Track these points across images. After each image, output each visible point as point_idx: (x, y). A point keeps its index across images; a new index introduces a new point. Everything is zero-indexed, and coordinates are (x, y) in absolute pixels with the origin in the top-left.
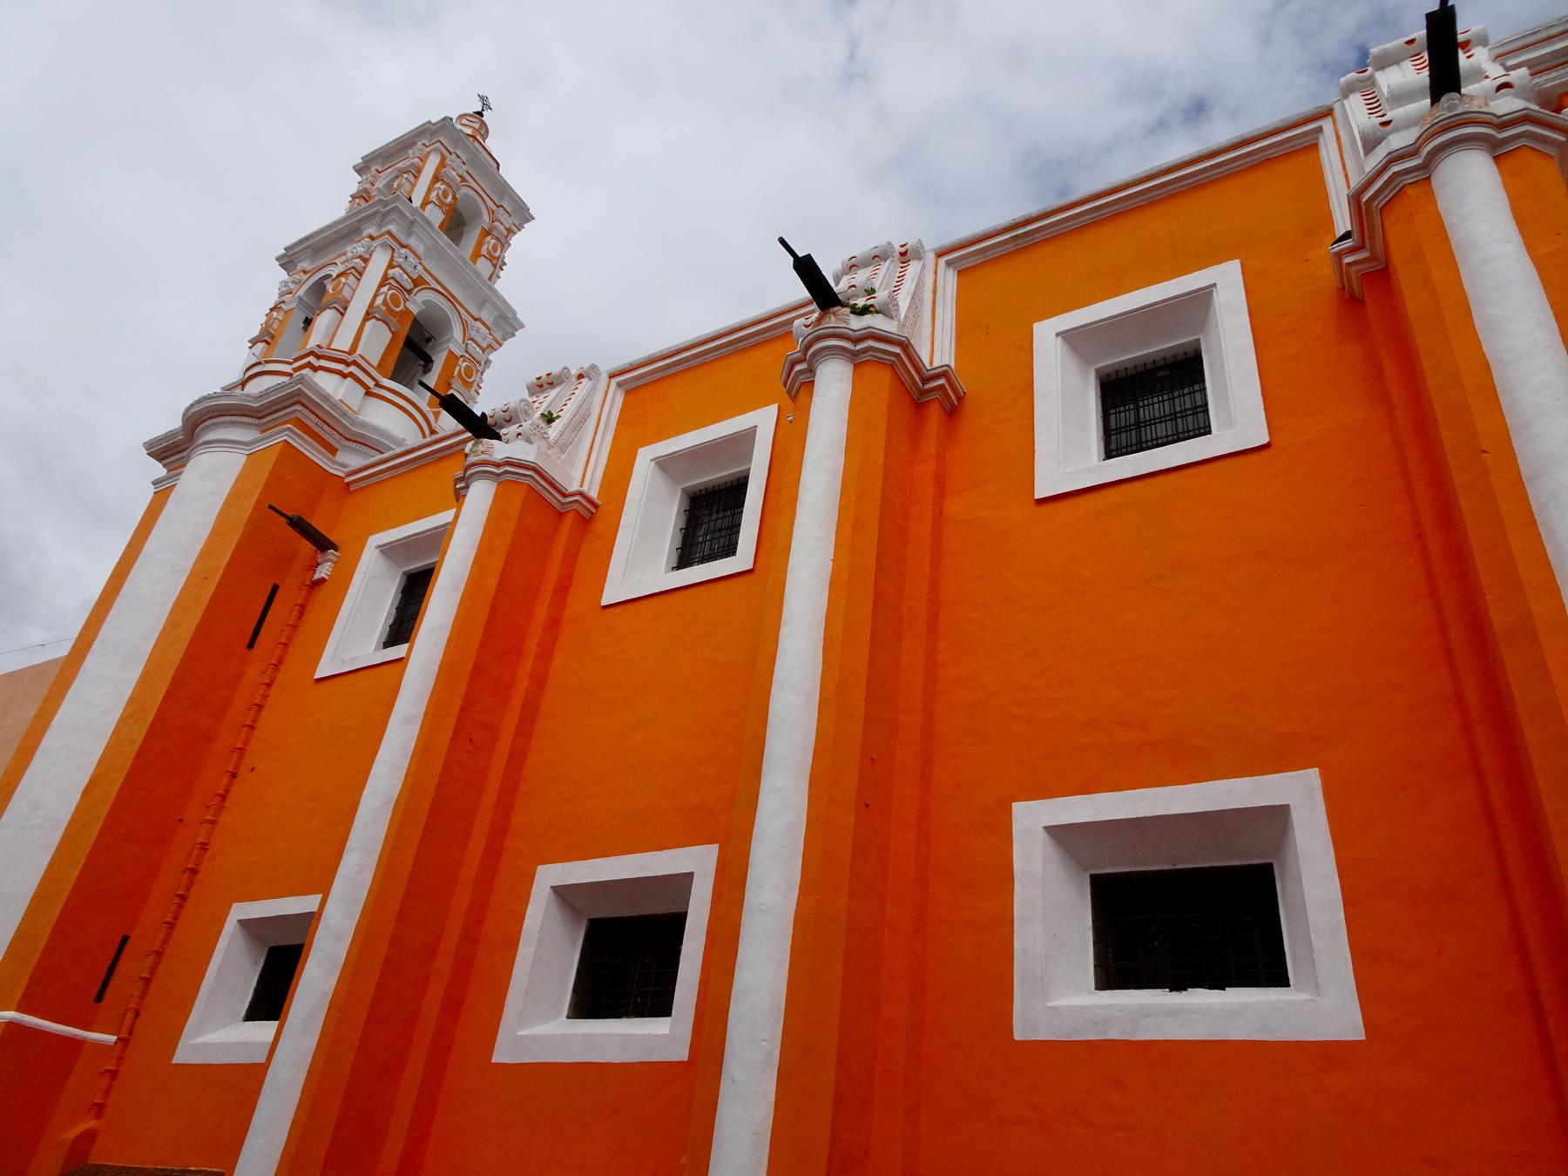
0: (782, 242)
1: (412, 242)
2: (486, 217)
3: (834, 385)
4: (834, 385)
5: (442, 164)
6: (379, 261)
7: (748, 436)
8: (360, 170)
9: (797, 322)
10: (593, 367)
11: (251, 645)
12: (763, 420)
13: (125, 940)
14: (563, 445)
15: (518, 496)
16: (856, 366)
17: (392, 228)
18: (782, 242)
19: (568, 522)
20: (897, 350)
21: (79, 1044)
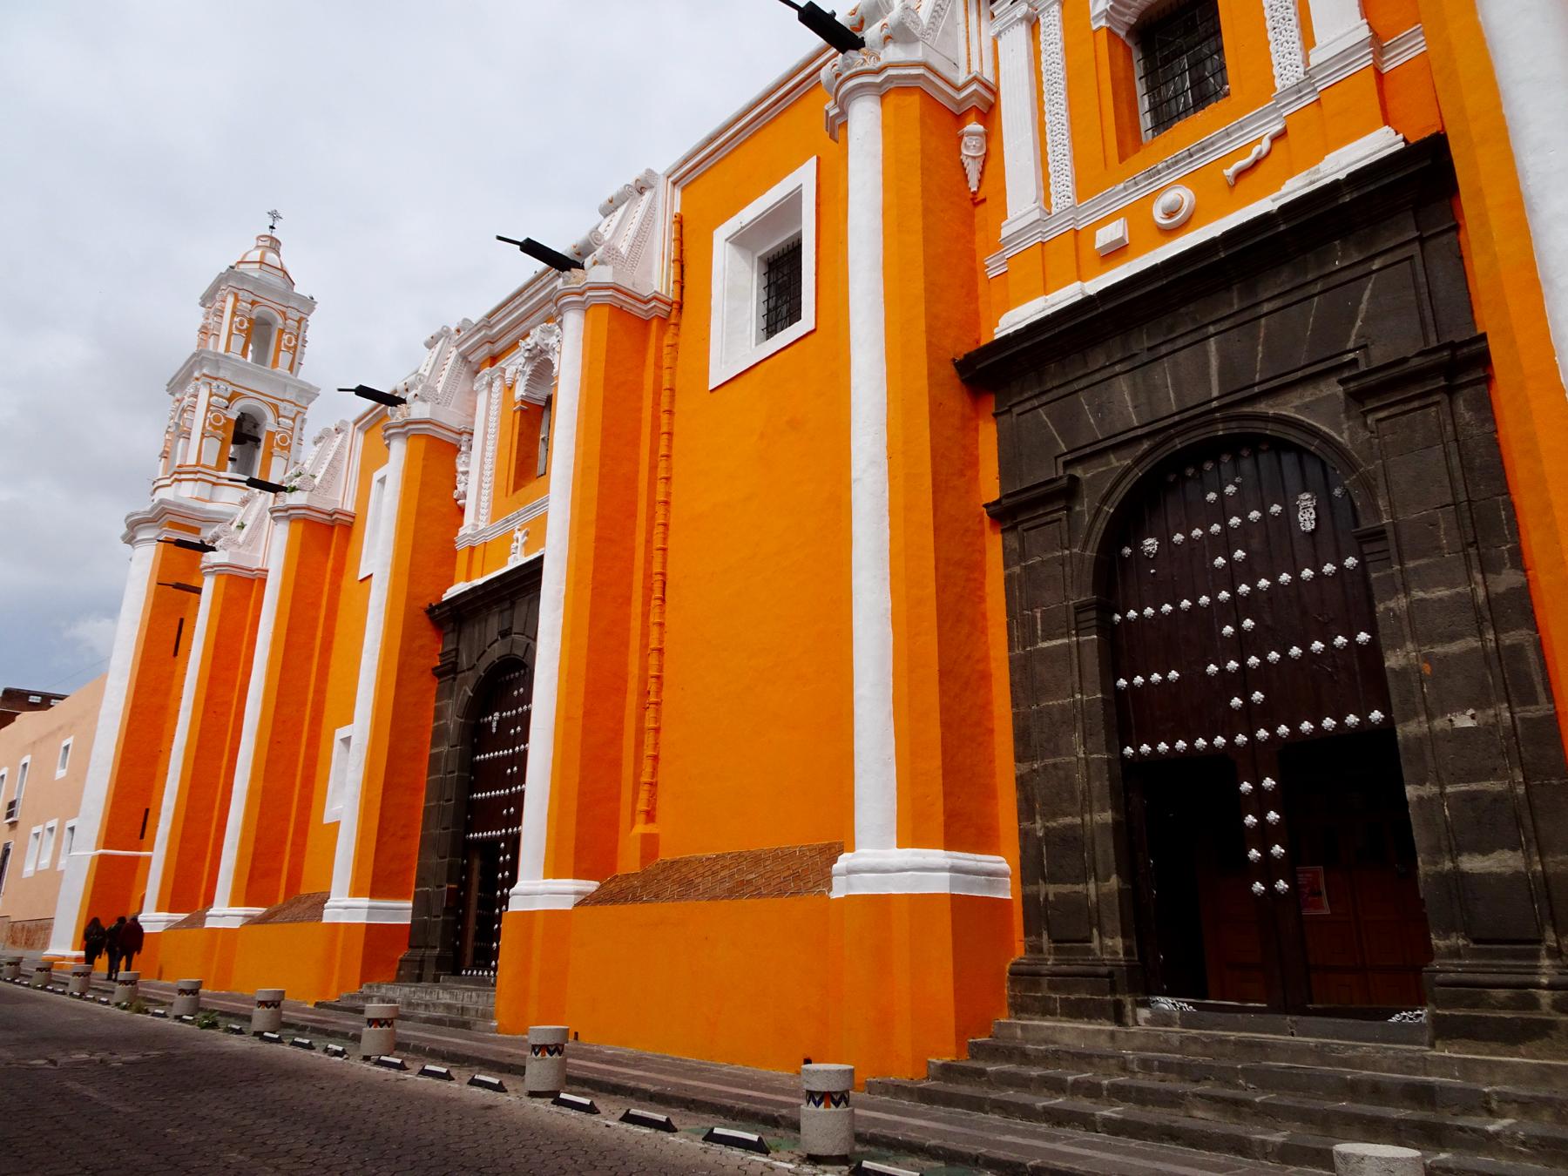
0: (500, 238)
1: (221, 375)
2: (280, 321)
3: (865, 118)
4: (865, 118)
5: (237, 299)
6: (204, 393)
7: (795, 199)
8: (203, 305)
9: (823, 72)
10: (650, 172)
11: (175, 654)
12: (804, 177)
13: (147, 811)
14: (249, 542)
15: (422, 444)
16: (882, 97)
17: (205, 371)
18: (500, 238)
19: (655, 324)
20: (921, 71)
21: (138, 857)
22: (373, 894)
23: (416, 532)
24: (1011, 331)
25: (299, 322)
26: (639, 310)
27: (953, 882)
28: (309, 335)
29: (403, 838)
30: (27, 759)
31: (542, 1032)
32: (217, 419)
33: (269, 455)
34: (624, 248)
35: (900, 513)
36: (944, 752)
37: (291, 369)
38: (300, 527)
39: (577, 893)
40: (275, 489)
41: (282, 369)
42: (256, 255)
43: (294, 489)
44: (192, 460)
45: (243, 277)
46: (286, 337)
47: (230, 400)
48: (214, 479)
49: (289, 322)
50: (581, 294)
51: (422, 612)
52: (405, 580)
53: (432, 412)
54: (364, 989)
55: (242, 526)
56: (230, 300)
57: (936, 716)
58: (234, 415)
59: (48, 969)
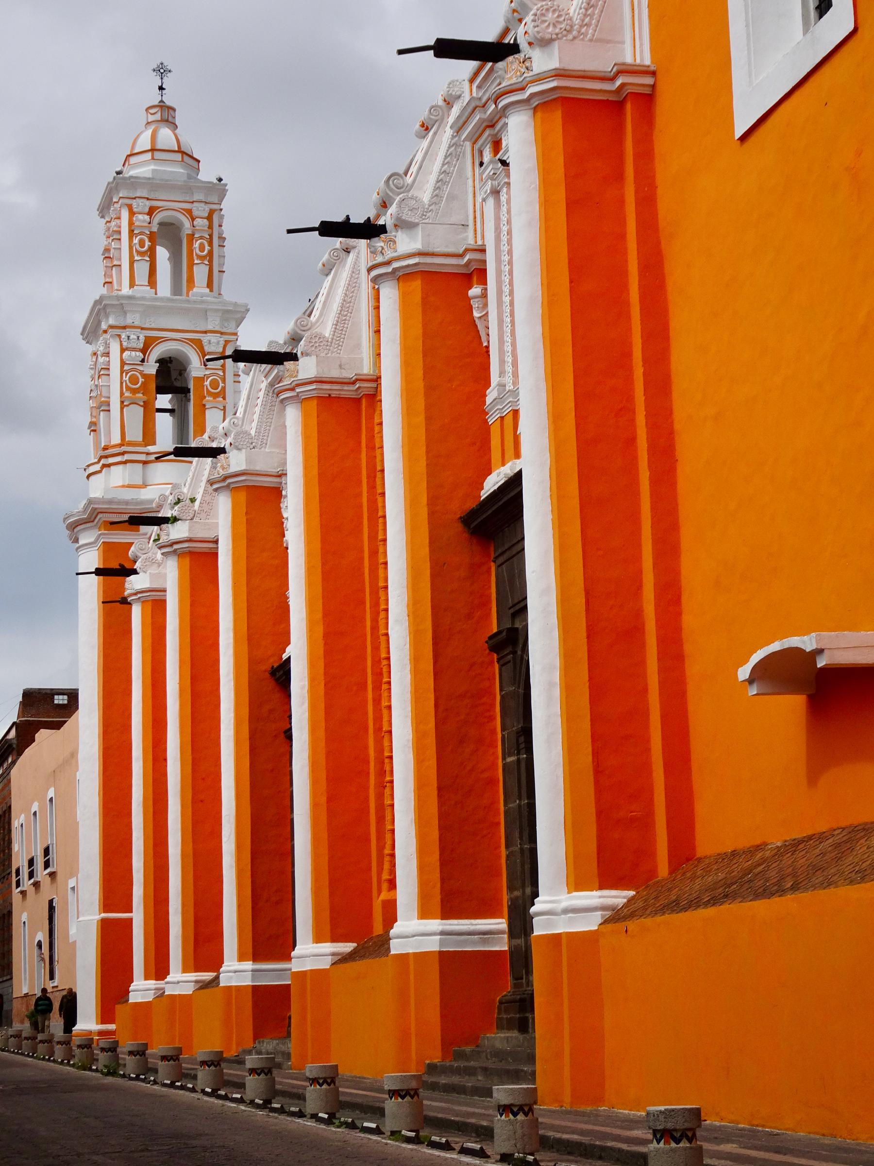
1: (129, 321)
2: (187, 224)
5: (132, 213)
8: (103, 217)
17: (112, 321)
22: (256, 958)
23: (249, 594)
24: (496, 487)
25: (210, 218)
26: (349, 391)
27: (441, 942)
28: (228, 229)
29: (277, 903)
30: (51, 793)
31: (311, 1069)
32: (134, 380)
33: (202, 409)
34: (327, 332)
35: (416, 659)
36: (442, 849)
37: (210, 285)
38: (187, 561)
39: (333, 954)
40: (214, 453)
41: (200, 289)
42: (144, 143)
43: (175, 519)
44: (116, 439)
45: (134, 182)
46: (196, 245)
47: (144, 351)
48: (143, 457)
49: (198, 222)
50: (293, 389)
51: (268, 675)
52: (245, 648)
53: (249, 460)
54: (257, 1045)
55: (193, 500)
56: (125, 214)
57: (435, 822)
58: (151, 368)
59: (688, 1134)
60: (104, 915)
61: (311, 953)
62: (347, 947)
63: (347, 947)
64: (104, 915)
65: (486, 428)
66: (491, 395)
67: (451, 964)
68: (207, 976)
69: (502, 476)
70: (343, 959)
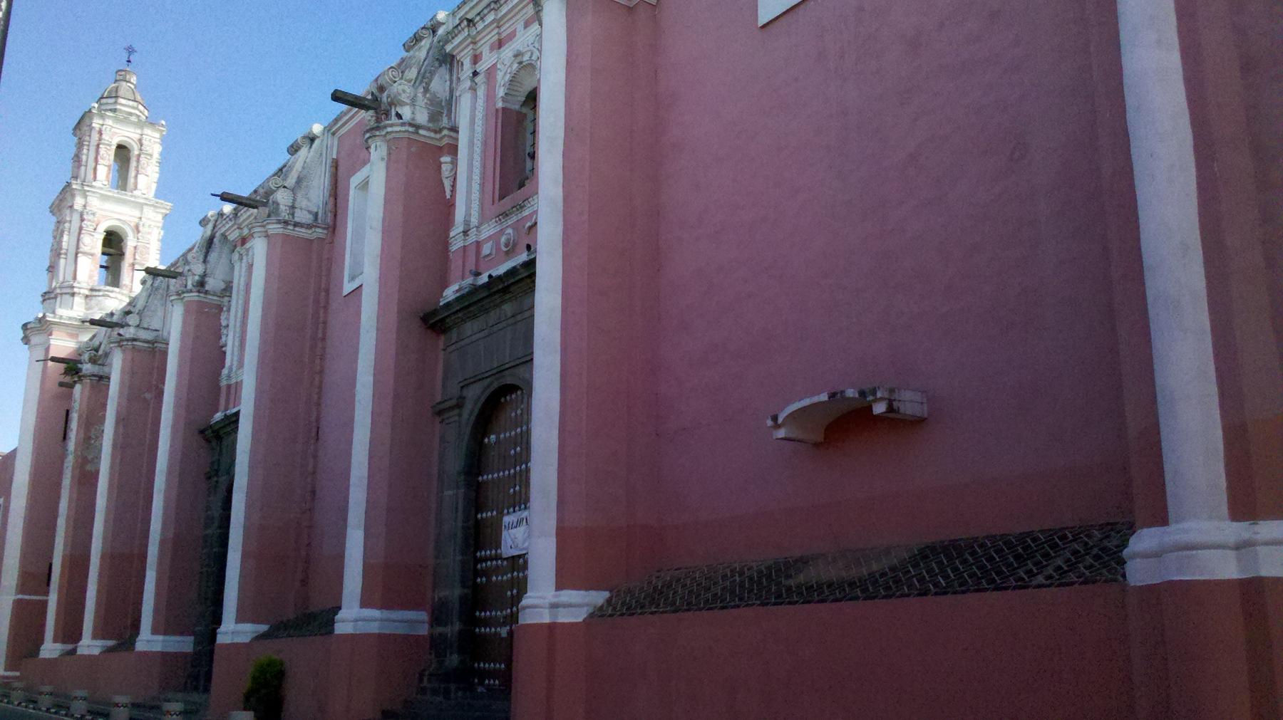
60: (20, 596)
61: (89, 645)
62: (110, 643)
63: (110, 643)
64: (20, 596)
65: (219, 388)
66: (225, 371)
67: (165, 658)
68: (70, 647)
69: (1257, 528)
70: (109, 650)
